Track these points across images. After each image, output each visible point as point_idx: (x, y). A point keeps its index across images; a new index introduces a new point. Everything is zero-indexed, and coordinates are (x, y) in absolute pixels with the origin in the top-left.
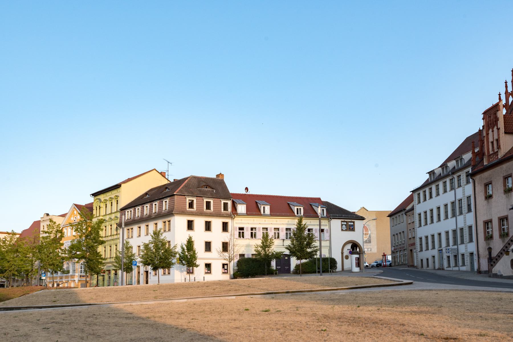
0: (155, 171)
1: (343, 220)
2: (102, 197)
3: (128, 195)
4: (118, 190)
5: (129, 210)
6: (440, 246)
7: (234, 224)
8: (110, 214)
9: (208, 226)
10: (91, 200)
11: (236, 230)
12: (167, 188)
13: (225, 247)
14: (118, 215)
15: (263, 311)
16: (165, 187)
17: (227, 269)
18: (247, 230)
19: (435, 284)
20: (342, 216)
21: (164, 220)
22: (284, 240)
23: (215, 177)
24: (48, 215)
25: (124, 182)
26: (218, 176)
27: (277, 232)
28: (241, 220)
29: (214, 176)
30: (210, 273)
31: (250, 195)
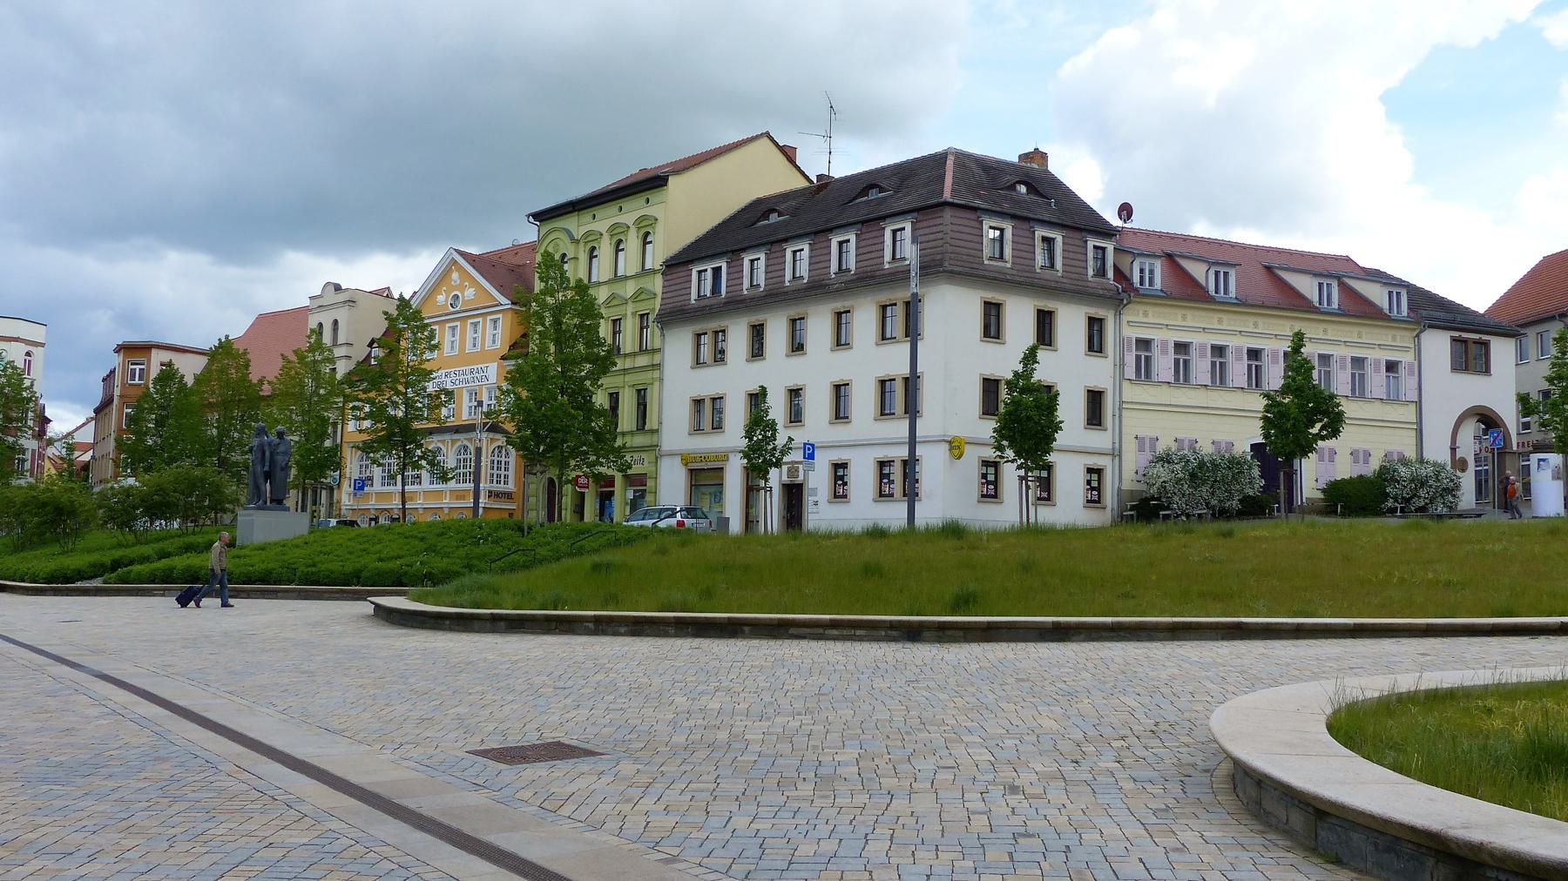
1: (1456, 334)
2: (576, 225)
3: (688, 211)
4: (654, 196)
14: (657, 284)
15: (483, 753)
16: (764, 207)
17: (1098, 489)
18: (1164, 352)
19: (1203, 643)
21: (698, 328)
23: (1016, 160)
24: (338, 288)
26: (1025, 157)
28: (1146, 314)
30: (1048, 499)
31: (1135, 232)
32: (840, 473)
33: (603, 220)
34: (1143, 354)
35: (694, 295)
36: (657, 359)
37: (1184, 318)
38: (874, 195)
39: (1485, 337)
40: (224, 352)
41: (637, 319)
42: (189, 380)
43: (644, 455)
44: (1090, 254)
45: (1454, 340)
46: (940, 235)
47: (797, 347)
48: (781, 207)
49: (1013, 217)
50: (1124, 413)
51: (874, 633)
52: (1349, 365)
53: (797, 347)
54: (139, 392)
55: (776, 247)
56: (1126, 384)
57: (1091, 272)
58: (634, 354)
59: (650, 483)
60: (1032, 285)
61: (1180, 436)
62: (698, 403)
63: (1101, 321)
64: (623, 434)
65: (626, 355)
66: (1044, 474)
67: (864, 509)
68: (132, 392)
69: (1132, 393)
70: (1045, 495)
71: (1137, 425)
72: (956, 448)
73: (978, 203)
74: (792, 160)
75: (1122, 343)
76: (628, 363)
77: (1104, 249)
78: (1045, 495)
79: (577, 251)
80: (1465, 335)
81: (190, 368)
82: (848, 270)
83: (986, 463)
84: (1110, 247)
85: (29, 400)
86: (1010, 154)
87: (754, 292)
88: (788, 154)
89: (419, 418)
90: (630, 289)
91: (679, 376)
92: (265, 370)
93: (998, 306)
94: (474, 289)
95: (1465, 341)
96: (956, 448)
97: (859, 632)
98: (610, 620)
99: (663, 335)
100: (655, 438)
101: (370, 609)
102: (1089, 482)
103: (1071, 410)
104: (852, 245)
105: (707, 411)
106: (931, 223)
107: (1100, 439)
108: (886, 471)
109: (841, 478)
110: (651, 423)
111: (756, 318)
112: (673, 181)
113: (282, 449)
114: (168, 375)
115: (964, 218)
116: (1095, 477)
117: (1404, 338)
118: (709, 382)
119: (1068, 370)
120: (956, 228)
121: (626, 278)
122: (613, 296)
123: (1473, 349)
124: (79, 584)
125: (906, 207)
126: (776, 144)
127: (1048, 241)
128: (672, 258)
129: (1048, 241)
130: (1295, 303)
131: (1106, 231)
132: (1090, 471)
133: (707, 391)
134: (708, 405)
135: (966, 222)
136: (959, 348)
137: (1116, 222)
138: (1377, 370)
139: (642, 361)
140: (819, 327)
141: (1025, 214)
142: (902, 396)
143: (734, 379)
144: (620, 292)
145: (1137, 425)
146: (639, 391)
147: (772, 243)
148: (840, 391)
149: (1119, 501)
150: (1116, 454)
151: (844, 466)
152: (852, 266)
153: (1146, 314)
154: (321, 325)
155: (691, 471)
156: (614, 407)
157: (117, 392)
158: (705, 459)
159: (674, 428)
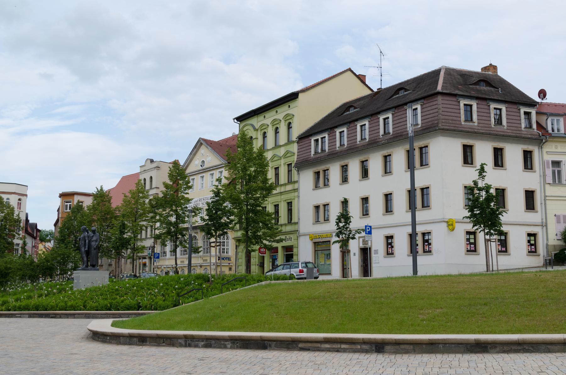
0: (349, 72)
2: (256, 122)
3: (306, 115)
4: (293, 104)
5: (319, 137)
6: (345, 253)
7: (544, 155)
8: (273, 148)
11: (548, 167)
12: (351, 106)
14: (294, 148)
16: (348, 105)
17: (535, 245)
24: (152, 161)
25: (303, 91)
26: (485, 69)
30: (506, 251)
32: (390, 241)
34: (556, 169)
35: (313, 152)
36: (296, 186)
38: (402, 93)
40: (101, 197)
41: (286, 167)
43: (292, 236)
46: (436, 110)
47: (345, 180)
49: (477, 98)
50: (547, 201)
51: (353, 347)
52: (551, 165)
53: (345, 180)
55: (352, 125)
56: (547, 186)
57: (523, 126)
58: (285, 185)
60: (490, 134)
61: (557, 214)
62: (317, 207)
63: (531, 152)
64: (281, 225)
65: (281, 185)
66: (503, 238)
69: (551, 191)
70: (504, 249)
71: (555, 209)
72: (450, 225)
73: (457, 92)
74: (363, 82)
75: (544, 164)
76: (283, 189)
77: (500, 110)
78: (504, 249)
79: (257, 135)
81: (88, 202)
82: (389, 133)
83: (468, 233)
84: (533, 112)
86: (476, 67)
87: (342, 148)
89: (184, 222)
90: (281, 151)
91: (307, 194)
92: (116, 202)
93: (471, 147)
94: (210, 158)
96: (450, 225)
97: (343, 346)
98: (193, 338)
99: (298, 174)
100: (296, 226)
102: (529, 241)
103: (515, 202)
104: (390, 120)
105: (321, 210)
106: (431, 104)
107: (532, 217)
108: (426, 238)
109: (391, 244)
110: (295, 220)
111: (343, 163)
112: (300, 95)
113: (94, 238)
115: (450, 101)
116: (532, 238)
118: (321, 196)
119: (512, 179)
120: (445, 106)
121: (280, 146)
122: (274, 156)
125: (418, 97)
127: (527, 114)
128: (302, 134)
129: (527, 114)
131: (531, 103)
132: (529, 235)
133: (321, 202)
135: (450, 102)
136: (447, 170)
137: (538, 100)
139: (289, 187)
140: (375, 163)
141: (484, 96)
142: (419, 198)
143: (333, 194)
144: (278, 154)
145: (555, 209)
146: (288, 203)
147: (350, 122)
148: (388, 197)
149: (548, 252)
150: (544, 225)
151: (392, 237)
155: (315, 243)
156: (277, 212)
158: (320, 237)
159: (306, 223)
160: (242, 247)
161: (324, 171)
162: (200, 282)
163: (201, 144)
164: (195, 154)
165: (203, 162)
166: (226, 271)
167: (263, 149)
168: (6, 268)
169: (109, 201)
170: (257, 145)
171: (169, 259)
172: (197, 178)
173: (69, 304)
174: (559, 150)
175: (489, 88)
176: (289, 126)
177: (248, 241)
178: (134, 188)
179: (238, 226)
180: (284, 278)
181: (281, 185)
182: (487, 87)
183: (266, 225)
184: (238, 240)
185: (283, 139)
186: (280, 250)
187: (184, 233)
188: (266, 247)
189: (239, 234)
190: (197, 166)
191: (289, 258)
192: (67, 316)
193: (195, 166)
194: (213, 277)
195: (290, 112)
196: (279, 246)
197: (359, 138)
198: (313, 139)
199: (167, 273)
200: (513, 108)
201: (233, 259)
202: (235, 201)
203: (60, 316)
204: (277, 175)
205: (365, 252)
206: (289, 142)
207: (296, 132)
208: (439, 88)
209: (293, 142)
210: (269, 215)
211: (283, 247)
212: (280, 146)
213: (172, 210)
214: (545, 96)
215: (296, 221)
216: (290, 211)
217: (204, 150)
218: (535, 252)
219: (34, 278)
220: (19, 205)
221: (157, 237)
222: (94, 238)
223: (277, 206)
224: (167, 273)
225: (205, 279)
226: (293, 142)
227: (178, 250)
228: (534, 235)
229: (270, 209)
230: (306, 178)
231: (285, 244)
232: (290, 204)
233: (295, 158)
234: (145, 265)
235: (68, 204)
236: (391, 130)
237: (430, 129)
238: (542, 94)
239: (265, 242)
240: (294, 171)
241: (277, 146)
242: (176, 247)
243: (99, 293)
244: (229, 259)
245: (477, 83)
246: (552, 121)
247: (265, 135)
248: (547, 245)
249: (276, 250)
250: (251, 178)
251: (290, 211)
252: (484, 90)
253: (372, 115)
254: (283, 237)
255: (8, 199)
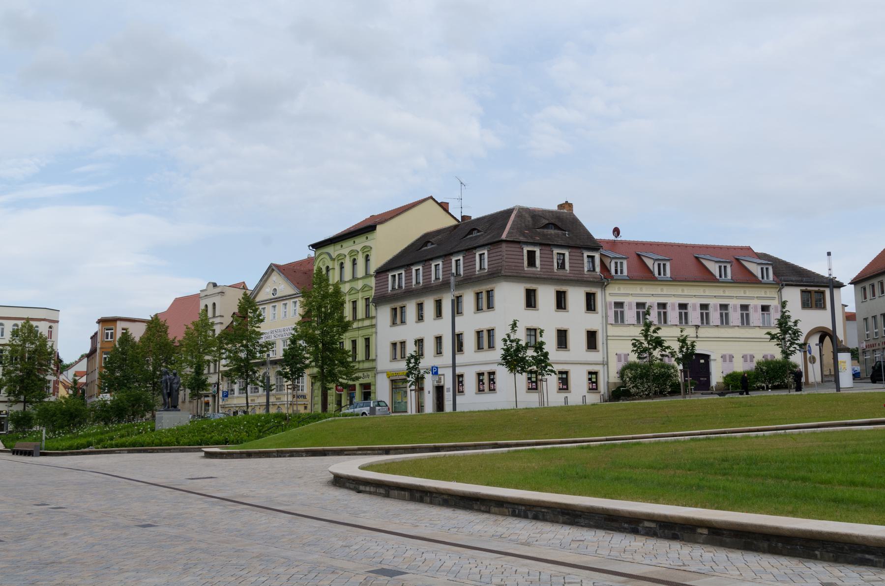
0: (431, 201)
1: (804, 288)
3: (387, 244)
5: (396, 273)
7: (606, 297)
8: (350, 281)
9: (561, 302)
10: (312, 253)
13: (592, 338)
14: (372, 282)
17: (596, 382)
20: (802, 281)
22: (697, 327)
24: (215, 285)
26: (561, 206)
27: (662, 311)
29: (554, 208)
30: (567, 389)
31: (622, 242)
33: (346, 248)
35: (390, 288)
36: (374, 321)
37: (641, 289)
39: (822, 289)
40: (155, 325)
42: (137, 339)
43: (369, 373)
44: (586, 260)
45: (802, 291)
47: (420, 318)
48: (432, 240)
49: (541, 244)
50: (609, 342)
53: (420, 318)
54: (112, 345)
55: (427, 263)
56: (609, 327)
57: (586, 269)
58: (363, 320)
59: (372, 388)
63: (594, 294)
64: (359, 362)
65: (359, 320)
66: (564, 376)
67: (261, 411)
68: (107, 345)
69: (613, 331)
70: (565, 387)
73: (522, 239)
74: (446, 210)
76: (360, 324)
77: (564, 254)
78: (565, 387)
80: (809, 288)
81: (137, 332)
84: (597, 256)
85: (50, 354)
86: (551, 205)
88: (444, 206)
89: (254, 358)
90: (359, 285)
91: (385, 331)
92: (176, 333)
93: (534, 291)
94: (283, 287)
95: (810, 292)
98: (282, 452)
101: (203, 454)
104: (461, 262)
105: (398, 347)
107: (593, 356)
110: (372, 356)
111: (419, 300)
112: (378, 227)
113: (176, 381)
114: (126, 338)
115: (514, 248)
116: (594, 376)
117: (772, 293)
121: (358, 279)
122: (352, 289)
123: (814, 296)
124: (83, 450)
126: (436, 202)
127: (592, 258)
130: (708, 278)
132: (590, 373)
133: (398, 339)
134: (398, 347)
138: (756, 311)
139: (367, 323)
143: (409, 332)
147: (426, 261)
150: (605, 364)
151: (494, 373)
152: (462, 273)
153: (619, 289)
154: (206, 306)
155: (392, 381)
157: (99, 346)
160: (318, 384)
161: (402, 308)
162: (279, 420)
163: (273, 270)
164: (266, 281)
165: (275, 290)
166: (301, 410)
167: (336, 286)
168: (76, 410)
169: (166, 332)
170: (334, 277)
171: (238, 397)
172: (269, 308)
173: (164, 440)
174: (622, 291)
175: (556, 231)
176: (367, 259)
177: (324, 378)
178: (197, 319)
179: (313, 364)
180: (351, 415)
181: (359, 320)
182: (557, 230)
183: (343, 363)
184: (314, 377)
185: (360, 272)
186: (358, 388)
187: (255, 369)
188: (342, 384)
189: (316, 370)
190: (268, 293)
191: (367, 396)
192: (164, 451)
193: (266, 293)
194: (290, 415)
195: (367, 244)
196: (357, 383)
197: (433, 278)
198: (390, 275)
199: (235, 413)
200: (576, 252)
201: (309, 397)
202: (311, 340)
203: (157, 451)
204: (355, 309)
205: (439, 390)
206: (367, 275)
207: (374, 266)
208: (504, 237)
209: (371, 276)
210: (346, 352)
211: (361, 385)
212: (358, 279)
213: (242, 346)
214: (618, 234)
215: (374, 358)
216: (368, 347)
217: (275, 277)
218: (596, 389)
219: (107, 421)
220: (50, 333)
221: (227, 374)
222: (176, 381)
223: (354, 342)
224: (235, 413)
225: (284, 417)
226: (371, 276)
227: (249, 387)
228: (596, 373)
229: (348, 346)
230: (383, 314)
231: (362, 381)
232: (367, 340)
233: (373, 293)
234: (207, 404)
235: (109, 332)
236: (462, 273)
237: (495, 275)
238: (616, 231)
239: (340, 380)
240: (372, 307)
241: (354, 279)
242: (247, 384)
243: (186, 431)
244: (304, 397)
245: (546, 226)
246: (616, 263)
247: (342, 266)
248: (608, 383)
249: (353, 388)
250: (328, 316)
251: (368, 347)
252: (551, 234)
253: (446, 256)
254: (360, 374)
255: (37, 327)
